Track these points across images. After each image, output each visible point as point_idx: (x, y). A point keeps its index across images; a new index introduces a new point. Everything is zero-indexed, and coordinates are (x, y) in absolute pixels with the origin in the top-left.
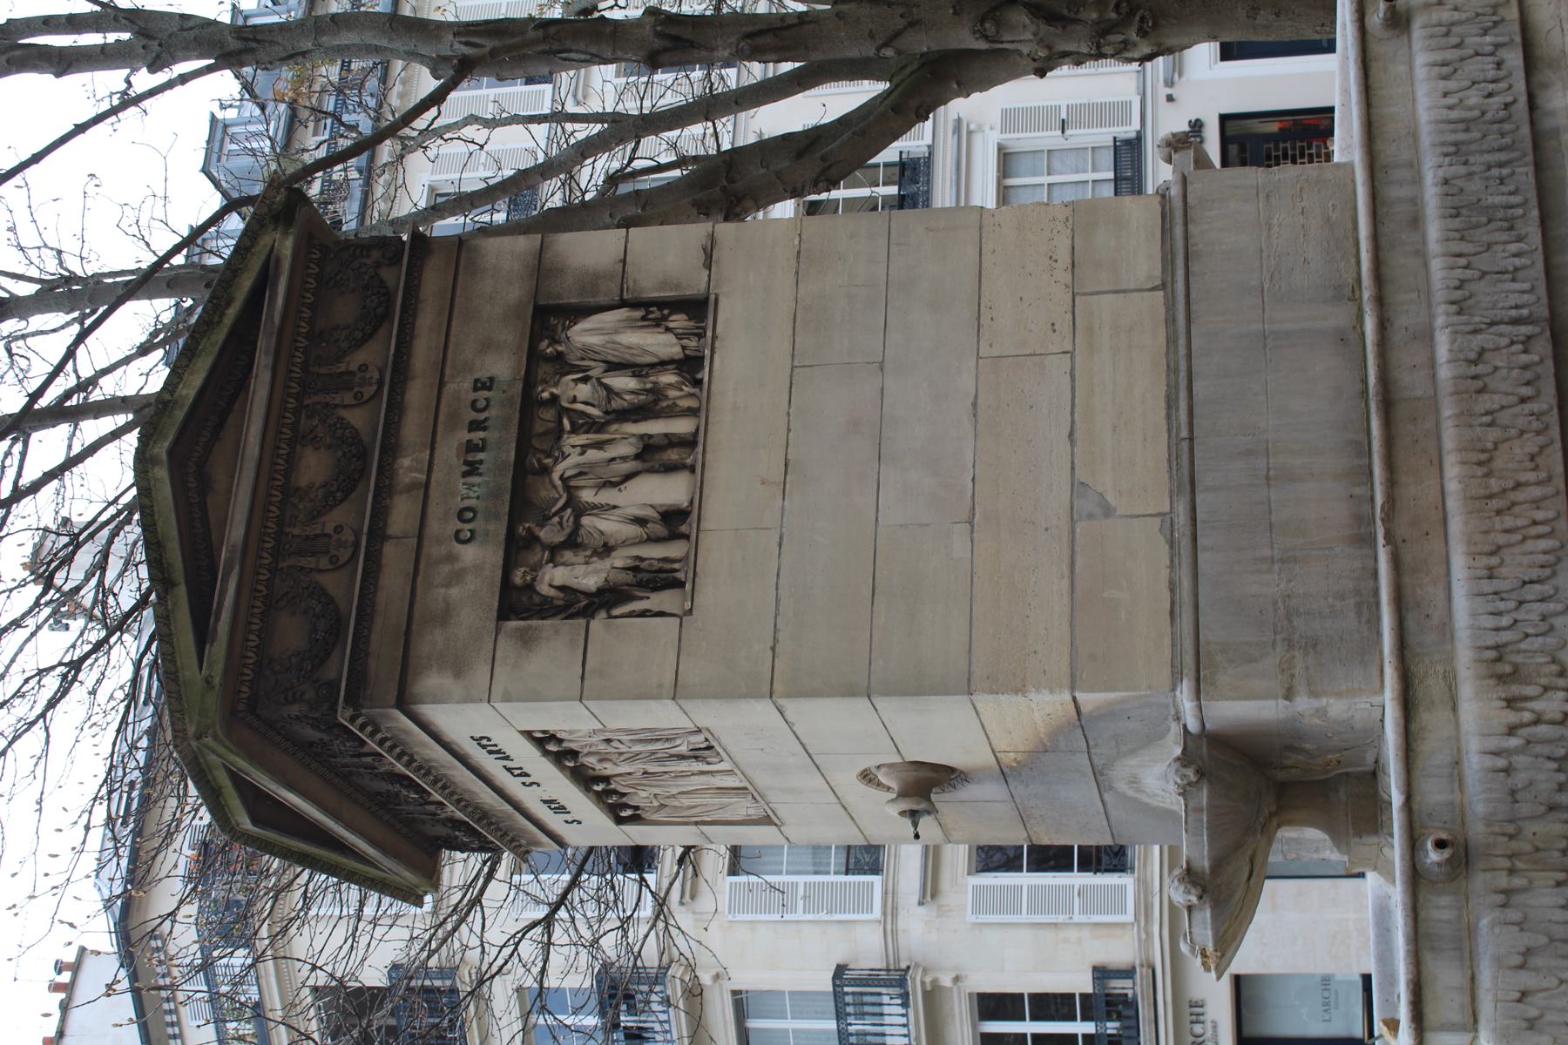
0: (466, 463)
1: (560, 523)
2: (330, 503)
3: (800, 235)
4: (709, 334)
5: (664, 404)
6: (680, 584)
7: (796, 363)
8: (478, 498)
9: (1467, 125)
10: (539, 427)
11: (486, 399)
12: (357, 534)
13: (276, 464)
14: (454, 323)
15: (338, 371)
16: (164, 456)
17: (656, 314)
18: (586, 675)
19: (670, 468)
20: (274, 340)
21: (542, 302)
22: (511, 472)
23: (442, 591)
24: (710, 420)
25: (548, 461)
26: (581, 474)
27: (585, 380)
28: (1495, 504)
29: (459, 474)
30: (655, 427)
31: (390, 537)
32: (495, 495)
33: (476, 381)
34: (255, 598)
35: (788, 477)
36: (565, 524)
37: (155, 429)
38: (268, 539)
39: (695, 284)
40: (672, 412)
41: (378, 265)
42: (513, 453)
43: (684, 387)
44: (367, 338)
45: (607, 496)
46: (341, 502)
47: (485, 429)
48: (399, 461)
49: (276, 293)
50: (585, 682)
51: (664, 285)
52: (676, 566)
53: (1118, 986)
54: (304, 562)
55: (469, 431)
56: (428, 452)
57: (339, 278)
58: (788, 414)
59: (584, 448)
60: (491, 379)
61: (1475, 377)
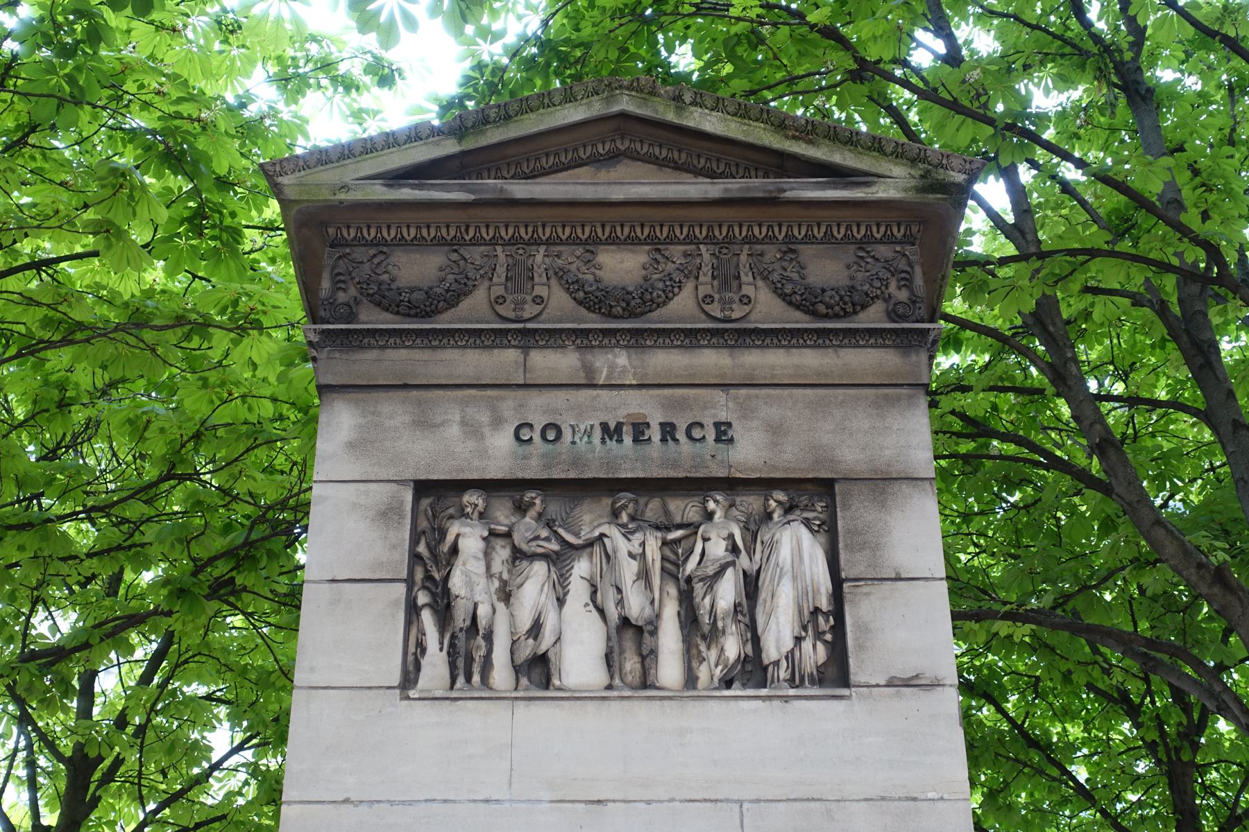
0: (619, 426)
1: (537, 538)
2: (573, 287)
3: (942, 799)
4: (792, 692)
5: (703, 648)
7: (745, 806)
8: (573, 443)
11: (704, 437)
13: (622, 226)
14: (809, 391)
15: (742, 274)
16: (616, 108)
18: (335, 585)
19: (610, 660)
20: (761, 195)
21: (837, 487)
22: (605, 476)
23: (457, 418)
24: (666, 703)
26: (608, 557)
27: (734, 549)
29: (604, 418)
30: (670, 638)
31: (526, 355)
32: (576, 462)
33: (729, 425)
34: (459, 227)
35: (583, 805)
36: (534, 543)
37: (650, 93)
38: (530, 230)
39: (858, 670)
40: (690, 657)
41: (887, 299)
42: (629, 475)
43: (720, 668)
44: (785, 297)
45: (578, 590)
46: (575, 299)
47: (663, 440)
48: (624, 352)
49: (824, 189)
50: (327, 585)
51: (864, 629)
52: (476, 678)
55: (661, 424)
56: (634, 382)
57: (869, 260)
58: (672, 800)
60: (731, 440)
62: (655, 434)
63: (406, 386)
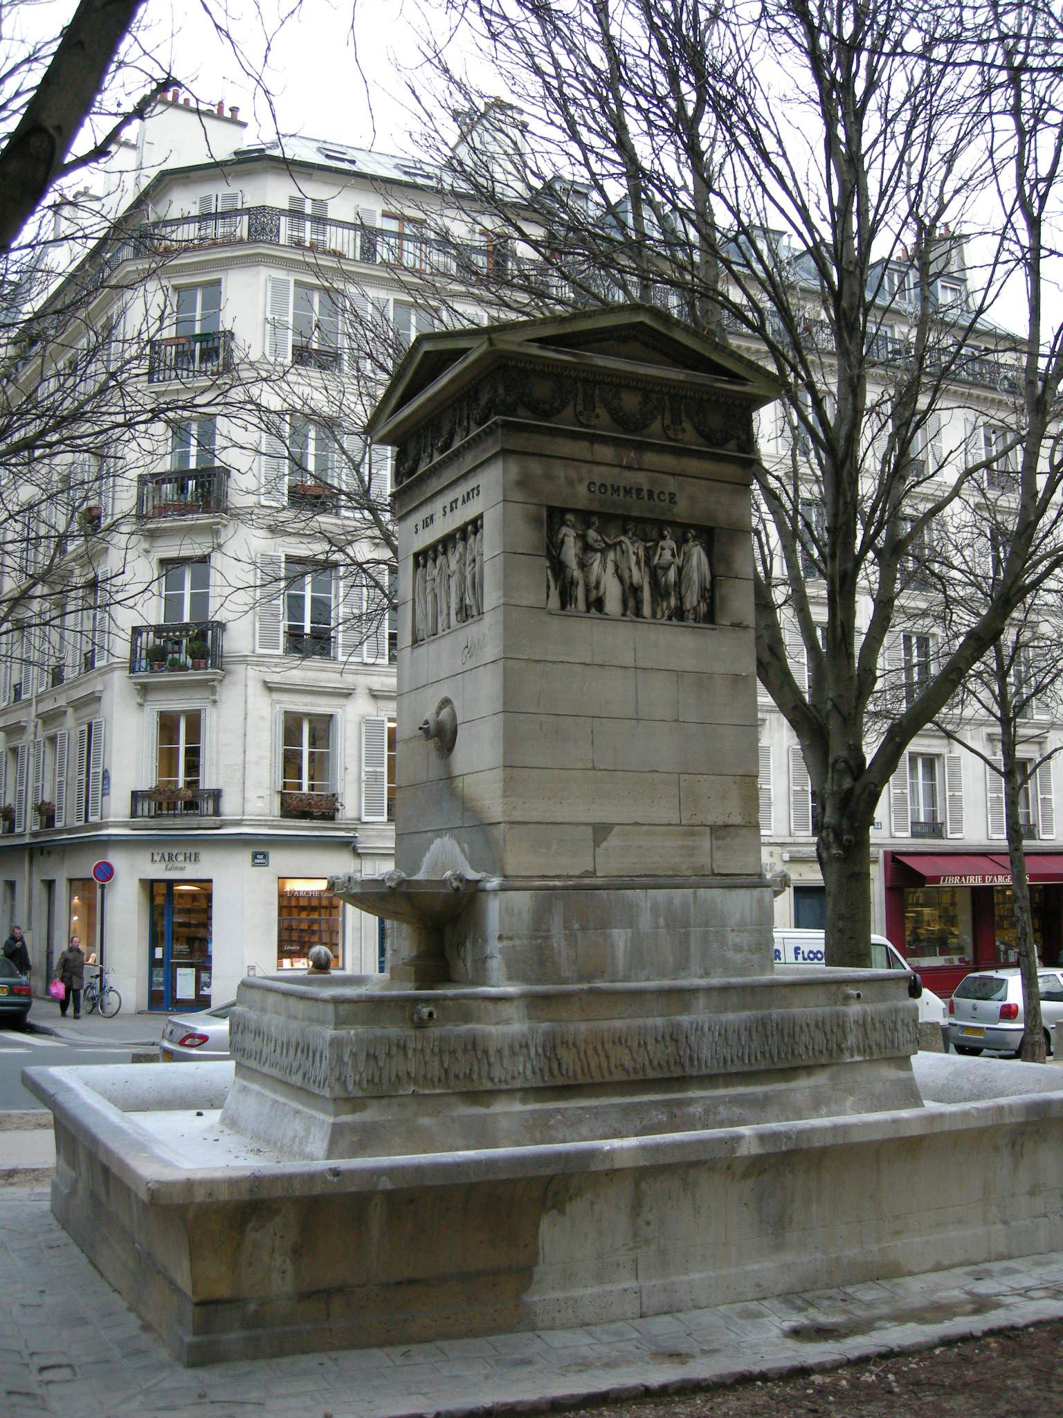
6: (563, 607)
9: (792, 1036)
10: (648, 529)
12: (595, 427)
17: (707, 595)
25: (630, 534)
27: (673, 555)
28: (599, 1047)
30: (646, 594)
40: (654, 603)
45: (610, 568)
53: (209, 806)
54: (580, 396)
59: (636, 554)
60: (675, 503)
61: (663, 1037)
62: (645, 494)
63: (541, 455)
